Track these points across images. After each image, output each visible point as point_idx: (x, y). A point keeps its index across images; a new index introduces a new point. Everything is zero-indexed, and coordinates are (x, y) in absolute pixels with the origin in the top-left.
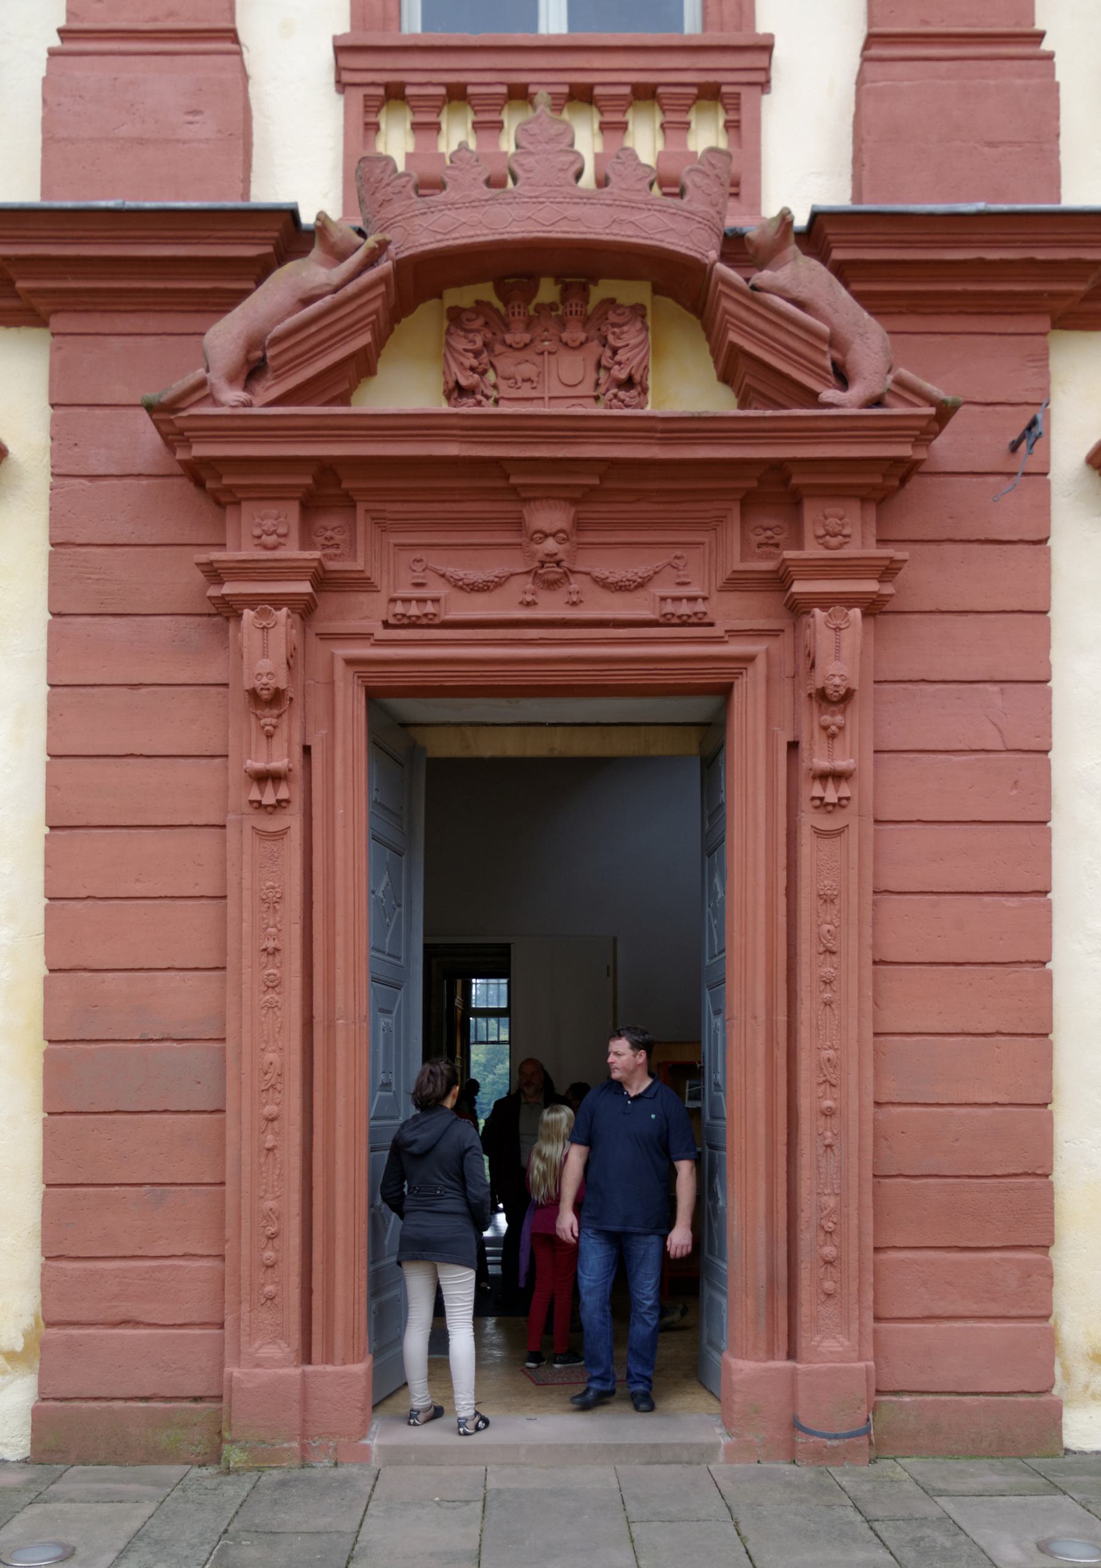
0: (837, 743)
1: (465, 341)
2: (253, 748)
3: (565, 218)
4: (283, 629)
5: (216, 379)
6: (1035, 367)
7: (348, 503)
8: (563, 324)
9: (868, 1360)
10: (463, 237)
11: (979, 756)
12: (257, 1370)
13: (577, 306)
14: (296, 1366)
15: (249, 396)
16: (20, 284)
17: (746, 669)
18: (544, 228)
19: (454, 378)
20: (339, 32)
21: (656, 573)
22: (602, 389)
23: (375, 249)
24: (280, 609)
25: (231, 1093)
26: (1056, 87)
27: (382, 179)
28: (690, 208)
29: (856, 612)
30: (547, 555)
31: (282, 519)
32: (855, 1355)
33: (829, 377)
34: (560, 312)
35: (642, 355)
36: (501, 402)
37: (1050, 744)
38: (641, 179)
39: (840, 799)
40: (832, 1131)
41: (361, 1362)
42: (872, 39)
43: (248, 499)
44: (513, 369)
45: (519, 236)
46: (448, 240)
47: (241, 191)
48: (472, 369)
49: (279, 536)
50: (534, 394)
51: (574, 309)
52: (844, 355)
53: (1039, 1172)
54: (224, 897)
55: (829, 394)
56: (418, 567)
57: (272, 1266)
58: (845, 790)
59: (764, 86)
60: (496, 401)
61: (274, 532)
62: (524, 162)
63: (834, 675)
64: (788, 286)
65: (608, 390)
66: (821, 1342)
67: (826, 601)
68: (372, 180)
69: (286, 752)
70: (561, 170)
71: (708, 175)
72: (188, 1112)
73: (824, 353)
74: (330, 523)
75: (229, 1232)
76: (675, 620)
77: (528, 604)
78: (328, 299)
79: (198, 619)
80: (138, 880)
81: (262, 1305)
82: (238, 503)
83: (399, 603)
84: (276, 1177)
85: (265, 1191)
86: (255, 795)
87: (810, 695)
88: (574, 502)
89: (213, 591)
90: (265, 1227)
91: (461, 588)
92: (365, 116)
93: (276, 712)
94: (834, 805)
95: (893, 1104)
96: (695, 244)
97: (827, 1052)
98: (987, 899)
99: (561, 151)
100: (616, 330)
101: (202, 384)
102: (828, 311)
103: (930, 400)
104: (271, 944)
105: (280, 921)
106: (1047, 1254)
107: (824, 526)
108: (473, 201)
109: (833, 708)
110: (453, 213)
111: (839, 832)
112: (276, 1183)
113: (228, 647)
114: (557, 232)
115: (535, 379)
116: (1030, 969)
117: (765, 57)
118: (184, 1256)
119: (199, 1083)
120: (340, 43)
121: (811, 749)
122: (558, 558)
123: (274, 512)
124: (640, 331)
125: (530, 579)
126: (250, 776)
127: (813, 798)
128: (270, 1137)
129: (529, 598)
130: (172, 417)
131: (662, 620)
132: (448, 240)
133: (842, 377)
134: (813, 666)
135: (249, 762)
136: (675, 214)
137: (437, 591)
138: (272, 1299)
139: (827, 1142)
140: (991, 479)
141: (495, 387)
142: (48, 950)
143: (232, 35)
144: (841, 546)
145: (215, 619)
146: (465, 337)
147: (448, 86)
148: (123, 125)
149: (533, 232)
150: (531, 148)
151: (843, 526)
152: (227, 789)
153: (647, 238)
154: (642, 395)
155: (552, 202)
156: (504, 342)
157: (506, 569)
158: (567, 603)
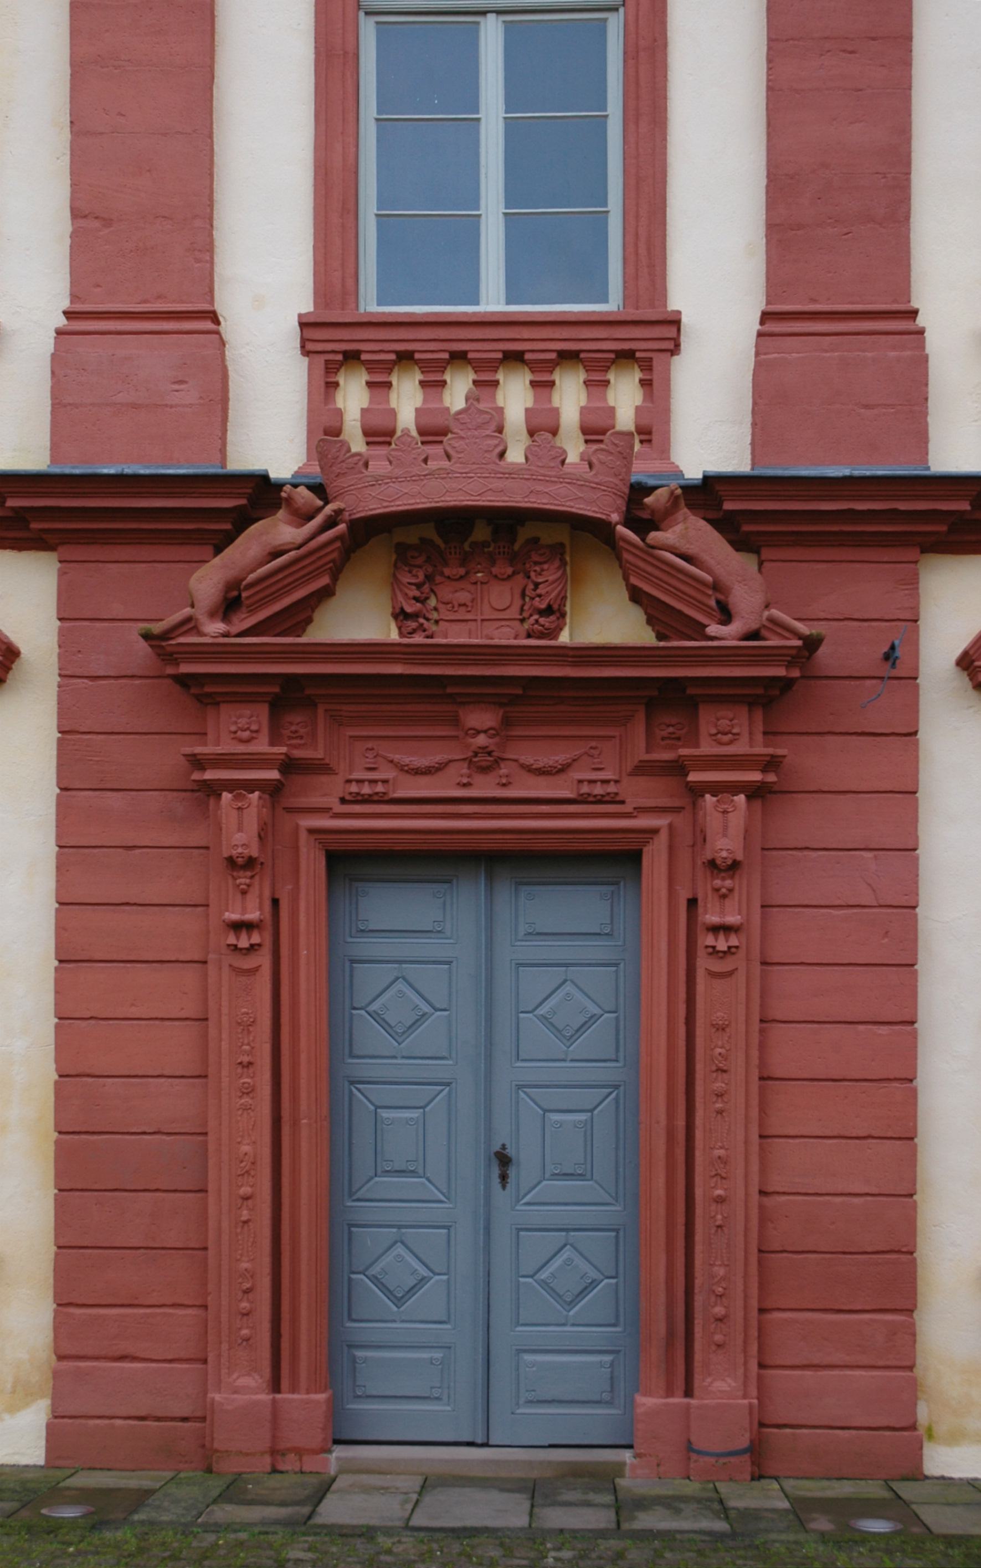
0: (727, 902)
1: (409, 575)
2: (230, 902)
3: (490, 489)
4: (255, 810)
5: (200, 613)
6: (907, 589)
7: (310, 704)
8: (493, 563)
9: (753, 1398)
10: (405, 505)
11: (855, 910)
12: (235, 1396)
13: (504, 547)
14: (267, 1394)
15: (228, 628)
16: (34, 525)
17: (652, 838)
18: (472, 498)
19: (399, 605)
20: (304, 310)
21: (574, 760)
22: (525, 614)
23: (331, 516)
24: (253, 792)
25: (212, 1175)
26: (925, 359)
27: (338, 457)
28: (596, 480)
29: (741, 798)
30: (480, 748)
31: (254, 718)
32: (740, 1393)
33: (714, 613)
34: (491, 549)
35: (559, 588)
36: (441, 623)
37: (917, 902)
38: (554, 458)
39: (729, 947)
40: (722, 1214)
41: (322, 1392)
42: (766, 317)
43: (224, 702)
44: (451, 595)
45: (452, 504)
46: (392, 506)
47: (219, 447)
48: (416, 599)
49: (252, 731)
50: (469, 617)
51: (502, 550)
52: (727, 597)
53: (904, 1249)
54: (206, 1019)
55: (714, 629)
56: (370, 755)
57: (247, 1314)
58: (734, 941)
59: (675, 349)
60: (437, 622)
61: (248, 729)
62: (456, 445)
63: (721, 850)
64: (677, 545)
65: (531, 615)
66: (712, 1383)
67: (717, 789)
68: (330, 456)
69: (257, 905)
70: (486, 451)
71: (612, 453)
72: (175, 1191)
73: (709, 596)
74: (295, 720)
75: (211, 1287)
76: (591, 799)
77: (465, 785)
78: (292, 554)
79: (183, 794)
80: (133, 1005)
81: (239, 1345)
82: (218, 704)
83: (354, 783)
84: (250, 1244)
85: (241, 1255)
86: (232, 940)
87: (704, 863)
88: (501, 705)
89: (196, 776)
90: (241, 1283)
91: (407, 772)
92: (327, 377)
93: (249, 874)
94: (724, 952)
95: (778, 1193)
96: (600, 508)
97: (718, 1151)
98: (861, 1028)
99: (487, 436)
100: (537, 568)
101: (189, 619)
102: (711, 562)
103: (800, 636)
104: (246, 1059)
105: (253, 1041)
106: (912, 1317)
107: (716, 726)
108: (414, 476)
109: (723, 874)
110: (396, 486)
111: (730, 974)
112: (250, 1249)
113: (208, 817)
114: (484, 501)
115: (470, 604)
116: (898, 1085)
117: (674, 329)
118: (174, 1305)
119: (185, 1168)
120: (304, 320)
121: (705, 906)
122: (489, 749)
123: (248, 712)
124: (559, 568)
125: (466, 765)
126: (228, 925)
127: (707, 947)
128: (245, 1212)
129: (465, 780)
130: (164, 644)
131: (580, 798)
132: (392, 506)
133: (725, 614)
134: (705, 840)
135: (227, 914)
136: (582, 485)
137: (387, 773)
138: (248, 1340)
139: (718, 1223)
140: (868, 683)
141: (436, 609)
142: (57, 1061)
143: (213, 317)
144: (730, 743)
145: (197, 794)
146: (410, 572)
147: (397, 353)
148: (119, 393)
149: (463, 501)
150: (462, 433)
151: (733, 726)
152: (208, 932)
153: (559, 505)
154: (561, 619)
155: (479, 477)
156: (442, 574)
157: (446, 756)
158: (498, 784)
